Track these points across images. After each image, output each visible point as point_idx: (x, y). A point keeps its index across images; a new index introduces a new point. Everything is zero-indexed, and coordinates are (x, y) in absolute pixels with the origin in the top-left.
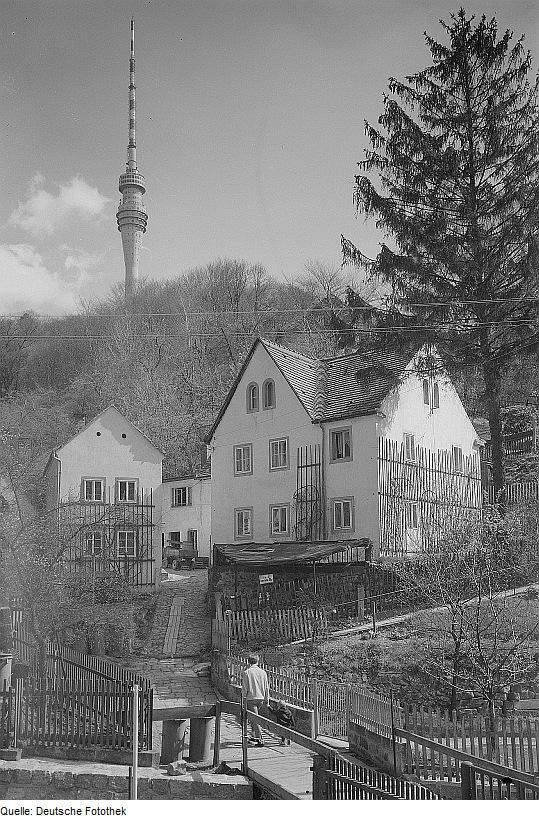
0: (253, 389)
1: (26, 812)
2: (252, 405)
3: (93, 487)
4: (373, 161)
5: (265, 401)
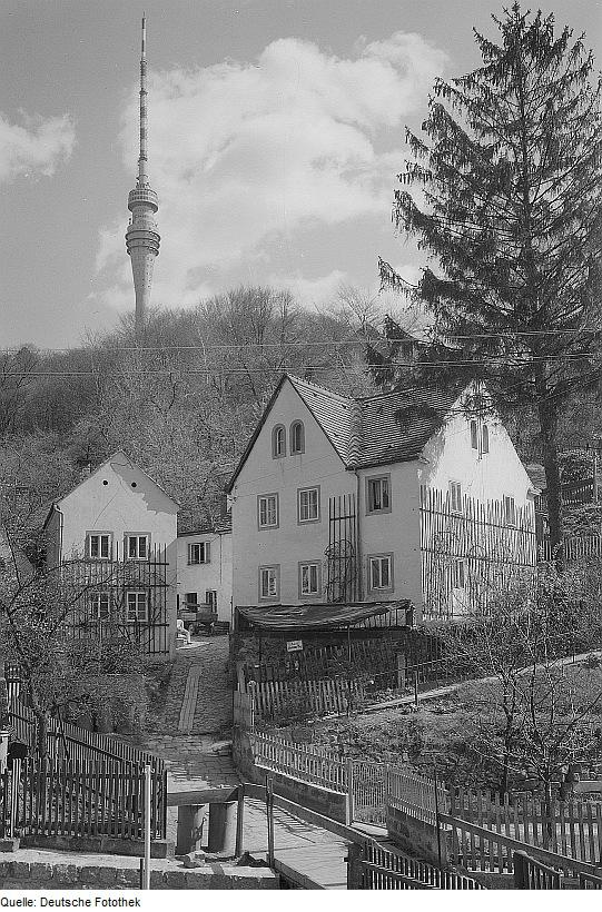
0: (279, 431)
1: (29, 903)
2: (278, 451)
3: (99, 543)
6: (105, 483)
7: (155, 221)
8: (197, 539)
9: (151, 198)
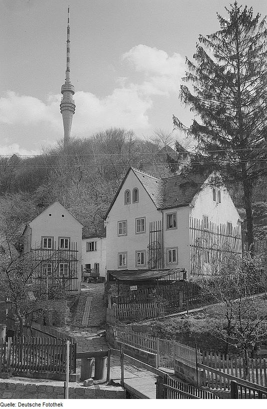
0: (127, 193)
1: (13, 405)
2: (127, 201)
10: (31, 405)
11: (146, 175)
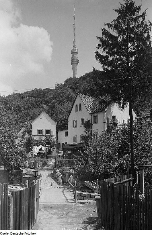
0: (77, 106)
1: (7, 234)
2: (77, 111)
3: (40, 132)
4: (99, 46)
5: (79, 109)
6: (41, 119)
7: (78, 57)
8: (95, 115)
9: (76, 51)
10: (18, 234)
11: (86, 96)
